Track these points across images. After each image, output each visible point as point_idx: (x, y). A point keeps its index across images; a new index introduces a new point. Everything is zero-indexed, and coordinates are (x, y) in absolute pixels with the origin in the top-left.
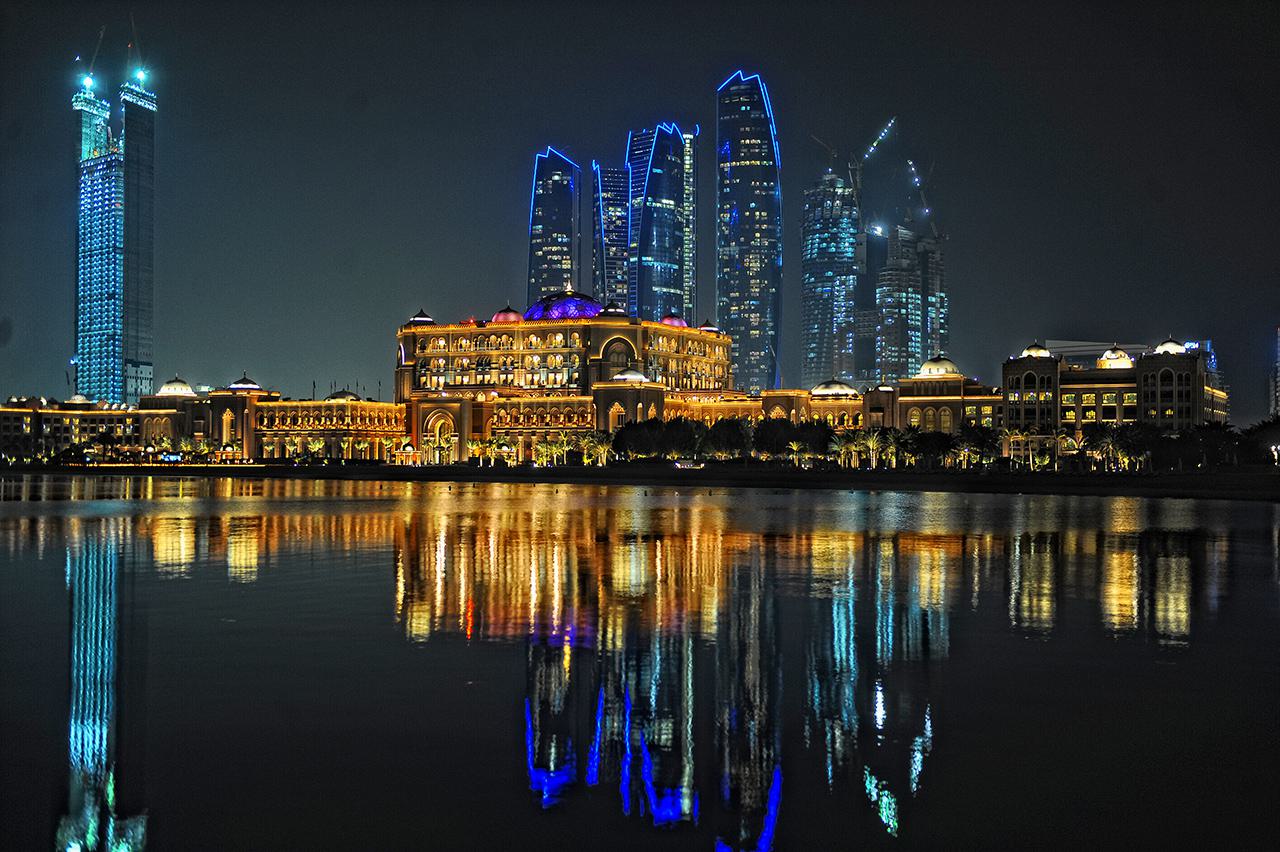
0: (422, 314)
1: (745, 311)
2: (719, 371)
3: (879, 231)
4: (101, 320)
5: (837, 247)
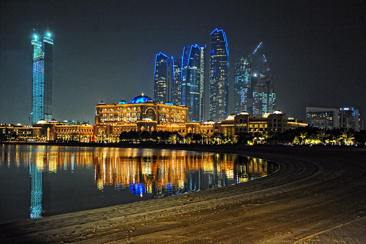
0: (102, 102)
1: (217, 99)
2: (183, 117)
3: (255, 75)
4: (38, 102)
5: (244, 80)
